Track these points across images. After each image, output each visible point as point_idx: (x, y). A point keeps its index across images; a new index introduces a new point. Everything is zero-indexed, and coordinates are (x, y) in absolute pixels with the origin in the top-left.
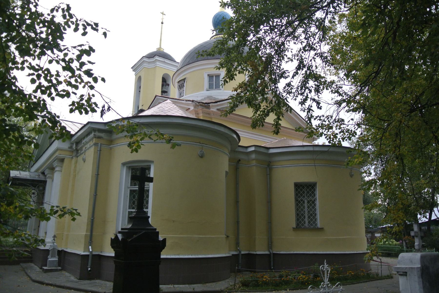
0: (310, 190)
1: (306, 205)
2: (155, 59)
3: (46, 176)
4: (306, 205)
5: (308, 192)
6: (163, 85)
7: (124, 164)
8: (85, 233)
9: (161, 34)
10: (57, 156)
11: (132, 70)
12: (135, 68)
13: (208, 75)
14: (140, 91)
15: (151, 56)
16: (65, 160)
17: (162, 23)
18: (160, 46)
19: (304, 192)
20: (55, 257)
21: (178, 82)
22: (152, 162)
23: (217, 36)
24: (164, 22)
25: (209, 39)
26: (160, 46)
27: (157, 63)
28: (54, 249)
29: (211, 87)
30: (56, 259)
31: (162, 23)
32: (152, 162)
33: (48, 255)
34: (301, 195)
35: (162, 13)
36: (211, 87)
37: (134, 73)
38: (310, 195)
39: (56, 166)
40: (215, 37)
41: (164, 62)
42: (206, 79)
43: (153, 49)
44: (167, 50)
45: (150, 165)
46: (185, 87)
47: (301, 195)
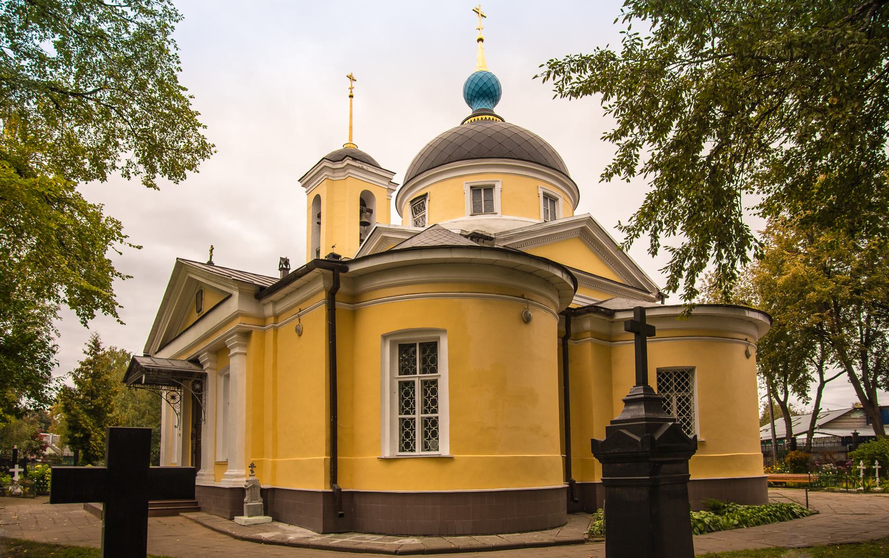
0: (683, 380)
1: (674, 403)
2: (345, 164)
3: (201, 366)
4: (674, 403)
5: (679, 384)
6: (361, 212)
7: (385, 337)
8: (323, 457)
9: (351, 117)
10: (238, 326)
11: (300, 184)
12: (306, 181)
13: (471, 187)
14: (319, 223)
15: (336, 158)
16: (253, 334)
17: (351, 96)
18: (351, 139)
19: (671, 384)
20: (256, 499)
21: (411, 202)
22: (444, 331)
23: (476, 118)
24: (354, 94)
25: (459, 124)
26: (351, 139)
27: (351, 171)
28: (254, 486)
29: (476, 211)
30: (259, 502)
31: (351, 96)
32: (444, 331)
33: (244, 496)
34: (668, 388)
35: (351, 78)
36: (476, 211)
37: (305, 189)
38: (683, 388)
39: (233, 347)
40: (472, 119)
41: (362, 169)
42: (468, 194)
43: (337, 146)
44: (364, 147)
45: (439, 338)
46: (427, 210)
47: (683, 388)
